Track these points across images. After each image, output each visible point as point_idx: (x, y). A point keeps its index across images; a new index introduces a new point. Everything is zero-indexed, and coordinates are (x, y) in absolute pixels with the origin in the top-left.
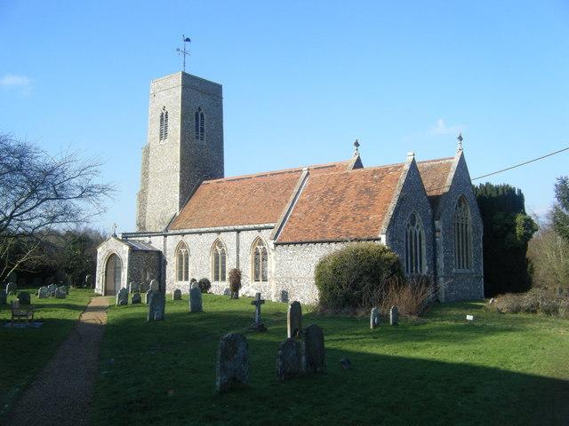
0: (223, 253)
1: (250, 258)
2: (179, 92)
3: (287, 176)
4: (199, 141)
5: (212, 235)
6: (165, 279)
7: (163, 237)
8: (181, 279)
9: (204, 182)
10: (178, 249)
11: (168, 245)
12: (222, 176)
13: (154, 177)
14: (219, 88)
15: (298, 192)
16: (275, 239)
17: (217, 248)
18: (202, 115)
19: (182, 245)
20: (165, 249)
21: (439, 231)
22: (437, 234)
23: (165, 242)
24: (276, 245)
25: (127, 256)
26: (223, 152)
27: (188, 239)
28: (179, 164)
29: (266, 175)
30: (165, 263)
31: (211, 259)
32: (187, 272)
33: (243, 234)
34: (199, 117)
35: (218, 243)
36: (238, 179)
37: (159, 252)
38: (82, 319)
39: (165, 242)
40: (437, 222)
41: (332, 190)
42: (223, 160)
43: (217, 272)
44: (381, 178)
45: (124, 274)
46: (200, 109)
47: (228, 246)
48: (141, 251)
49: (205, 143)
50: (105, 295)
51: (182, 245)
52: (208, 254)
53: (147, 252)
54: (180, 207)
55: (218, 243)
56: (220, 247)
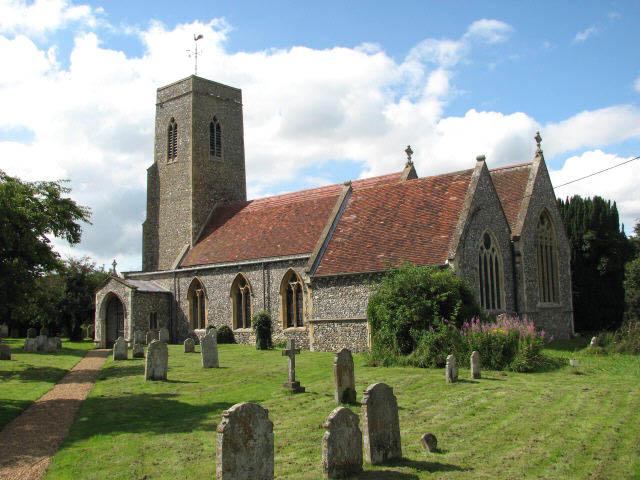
14: (239, 91)
44: (444, 190)
46: (215, 119)
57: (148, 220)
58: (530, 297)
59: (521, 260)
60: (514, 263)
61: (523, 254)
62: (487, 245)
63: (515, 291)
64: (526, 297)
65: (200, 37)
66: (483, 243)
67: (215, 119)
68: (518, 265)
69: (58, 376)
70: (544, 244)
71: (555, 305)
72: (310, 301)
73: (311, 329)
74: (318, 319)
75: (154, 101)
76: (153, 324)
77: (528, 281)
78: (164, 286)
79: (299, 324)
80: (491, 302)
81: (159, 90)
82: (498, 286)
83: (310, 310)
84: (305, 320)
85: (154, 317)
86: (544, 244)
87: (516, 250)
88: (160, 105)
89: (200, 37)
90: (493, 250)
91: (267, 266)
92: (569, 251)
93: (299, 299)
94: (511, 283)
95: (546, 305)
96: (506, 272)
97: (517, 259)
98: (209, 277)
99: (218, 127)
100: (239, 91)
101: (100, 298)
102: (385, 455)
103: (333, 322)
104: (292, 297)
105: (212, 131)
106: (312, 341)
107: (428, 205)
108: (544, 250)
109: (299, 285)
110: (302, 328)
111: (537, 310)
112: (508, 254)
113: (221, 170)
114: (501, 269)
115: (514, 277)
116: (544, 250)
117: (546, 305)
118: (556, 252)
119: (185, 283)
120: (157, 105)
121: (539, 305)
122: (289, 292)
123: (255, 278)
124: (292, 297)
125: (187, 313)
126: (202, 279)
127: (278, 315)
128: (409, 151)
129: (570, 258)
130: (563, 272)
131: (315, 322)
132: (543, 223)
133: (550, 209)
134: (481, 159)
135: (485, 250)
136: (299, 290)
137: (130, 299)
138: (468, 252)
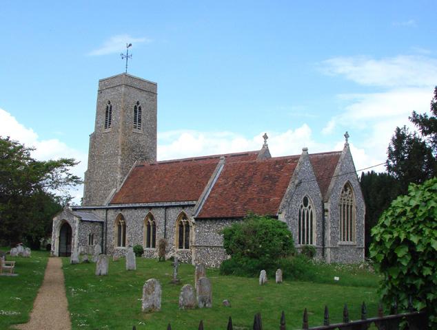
0: (154, 225)
1: (177, 229)
14: (155, 85)
17: (149, 220)
40: (325, 204)
42: (156, 146)
44: (281, 168)
46: (138, 103)
50: (59, 256)
57: (89, 170)
58: (333, 238)
59: (328, 217)
60: (324, 216)
61: (329, 210)
62: (306, 204)
63: (323, 234)
64: (330, 237)
65: (130, 45)
66: (302, 203)
67: (138, 103)
68: (326, 217)
69: (207, 191)
70: (350, 204)
71: (351, 243)
72: (194, 233)
73: (193, 250)
74: (198, 245)
75: (97, 88)
76: (91, 242)
77: (332, 227)
78: (100, 216)
79: (187, 247)
80: (306, 240)
81: (101, 81)
82: (311, 230)
83: (194, 238)
84: (190, 245)
85: (91, 237)
86: (350, 204)
87: (325, 208)
88: (100, 92)
89: (130, 45)
90: (310, 207)
91: (167, 207)
92: (364, 209)
93: (187, 231)
94: (321, 229)
95: (345, 243)
96: (318, 221)
97: (326, 214)
98: (130, 212)
99: (140, 108)
100: (155, 85)
101: (56, 222)
102: (205, 305)
103: (207, 247)
104: (184, 230)
105: (136, 111)
106: (194, 258)
107: (271, 178)
108: (346, 208)
109: (187, 222)
110: (189, 250)
111: (337, 246)
112: (320, 210)
113: (140, 138)
114: (314, 219)
115: (323, 224)
116: (346, 208)
117: (345, 243)
118: (354, 209)
119: (112, 216)
120: (99, 91)
121: (339, 243)
122: (181, 226)
123: (159, 215)
124: (184, 230)
125: (99, 53)
126: (125, 213)
127: (174, 239)
128: (265, 137)
129: (365, 213)
130: (359, 222)
131: (196, 246)
132: (346, 190)
133: (352, 182)
134: (305, 150)
135: (304, 207)
136: (188, 226)
137: (77, 225)
138: (292, 208)
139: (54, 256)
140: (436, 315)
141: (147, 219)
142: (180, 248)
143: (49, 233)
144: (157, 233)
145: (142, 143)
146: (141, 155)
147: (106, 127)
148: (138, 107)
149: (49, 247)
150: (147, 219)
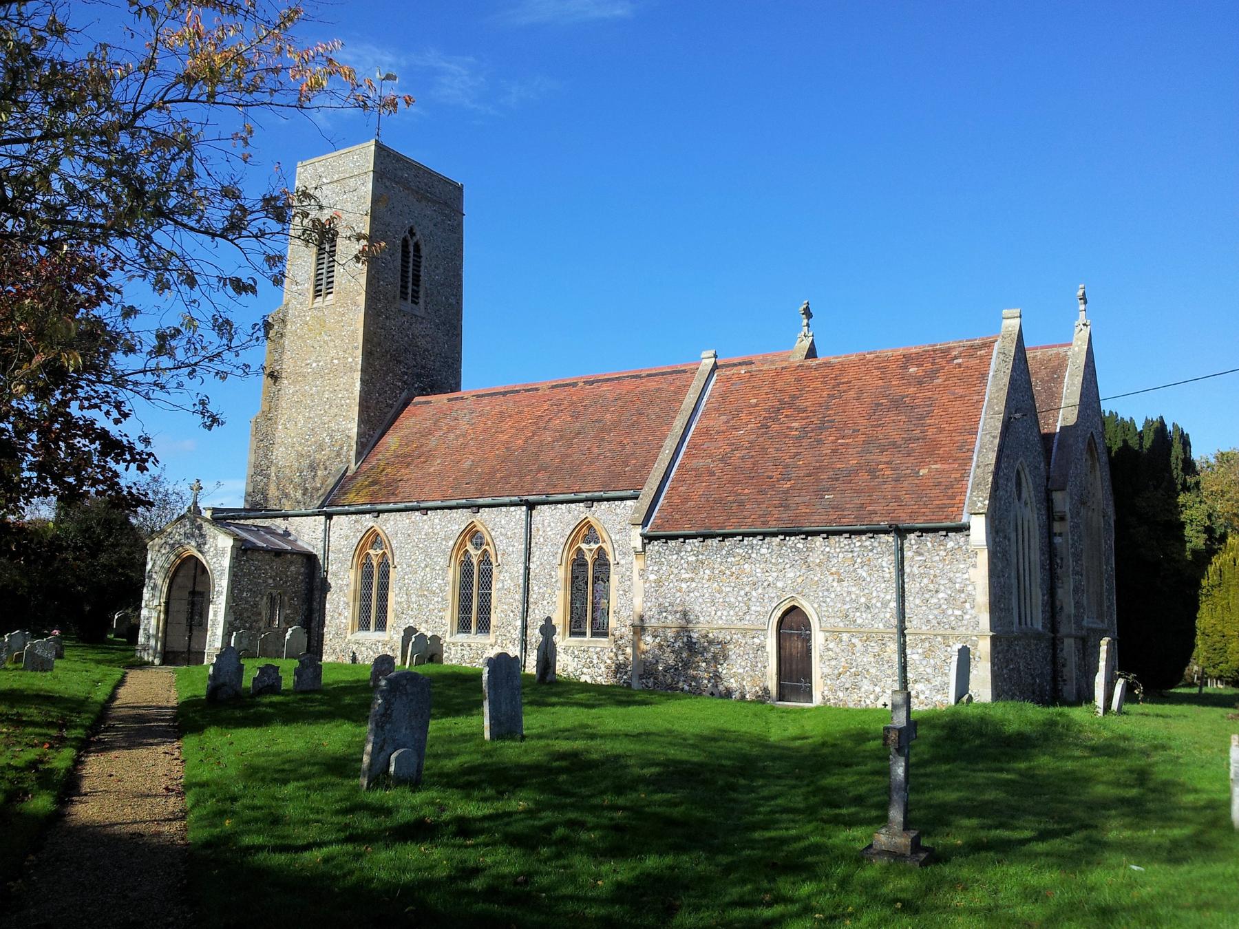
0: (486, 560)
1: (561, 574)
2: (367, 188)
3: (627, 385)
4: (408, 305)
5: (455, 514)
6: (322, 624)
7: (322, 518)
8: (364, 625)
9: (416, 399)
10: (361, 549)
11: (333, 538)
12: (456, 387)
13: (295, 382)
14: (460, 189)
15: (695, 410)
16: (644, 524)
17: (470, 547)
18: (417, 247)
19: (374, 539)
20: (326, 551)
21: (1062, 519)
22: (1057, 527)
23: (327, 531)
24: (648, 539)
25: (226, 562)
26: (459, 335)
27: (392, 526)
28: (359, 352)
29: (574, 385)
30: (325, 587)
31: (452, 575)
32: (383, 609)
33: (543, 514)
34: (410, 252)
35: (472, 534)
36: (504, 394)
37: (310, 558)
38: (984, 511)
39: (327, 531)
40: (1057, 496)
41: (790, 403)
42: (460, 353)
43: (465, 608)
44: (932, 375)
45: (217, 612)
46: (412, 233)
47: (501, 544)
48: (265, 550)
49: (420, 310)
50: (164, 662)
51: (374, 539)
52: (442, 561)
53: (279, 553)
54: (359, 454)
55: (472, 534)
56: (478, 546)
68: (1058, 540)
109: (600, 548)
139: (143, 665)
140: (1, 733)
141: (463, 544)
142: (572, 634)
143: (132, 596)
144: (496, 585)
145: (422, 343)
146: (419, 376)
147: (317, 293)
148: (411, 243)
149: (132, 632)
150: (463, 544)
